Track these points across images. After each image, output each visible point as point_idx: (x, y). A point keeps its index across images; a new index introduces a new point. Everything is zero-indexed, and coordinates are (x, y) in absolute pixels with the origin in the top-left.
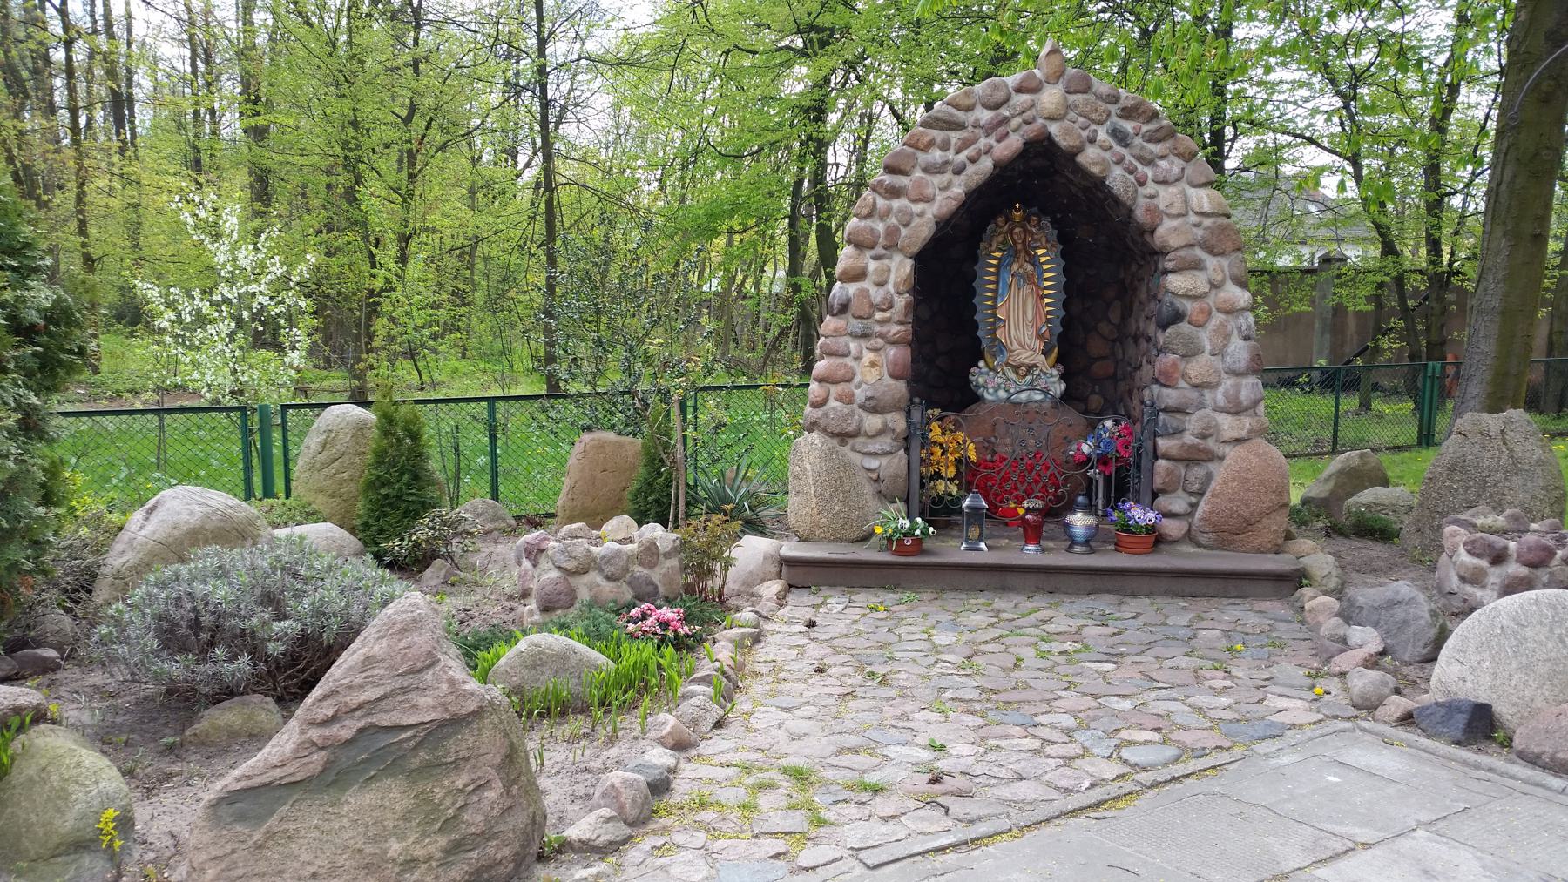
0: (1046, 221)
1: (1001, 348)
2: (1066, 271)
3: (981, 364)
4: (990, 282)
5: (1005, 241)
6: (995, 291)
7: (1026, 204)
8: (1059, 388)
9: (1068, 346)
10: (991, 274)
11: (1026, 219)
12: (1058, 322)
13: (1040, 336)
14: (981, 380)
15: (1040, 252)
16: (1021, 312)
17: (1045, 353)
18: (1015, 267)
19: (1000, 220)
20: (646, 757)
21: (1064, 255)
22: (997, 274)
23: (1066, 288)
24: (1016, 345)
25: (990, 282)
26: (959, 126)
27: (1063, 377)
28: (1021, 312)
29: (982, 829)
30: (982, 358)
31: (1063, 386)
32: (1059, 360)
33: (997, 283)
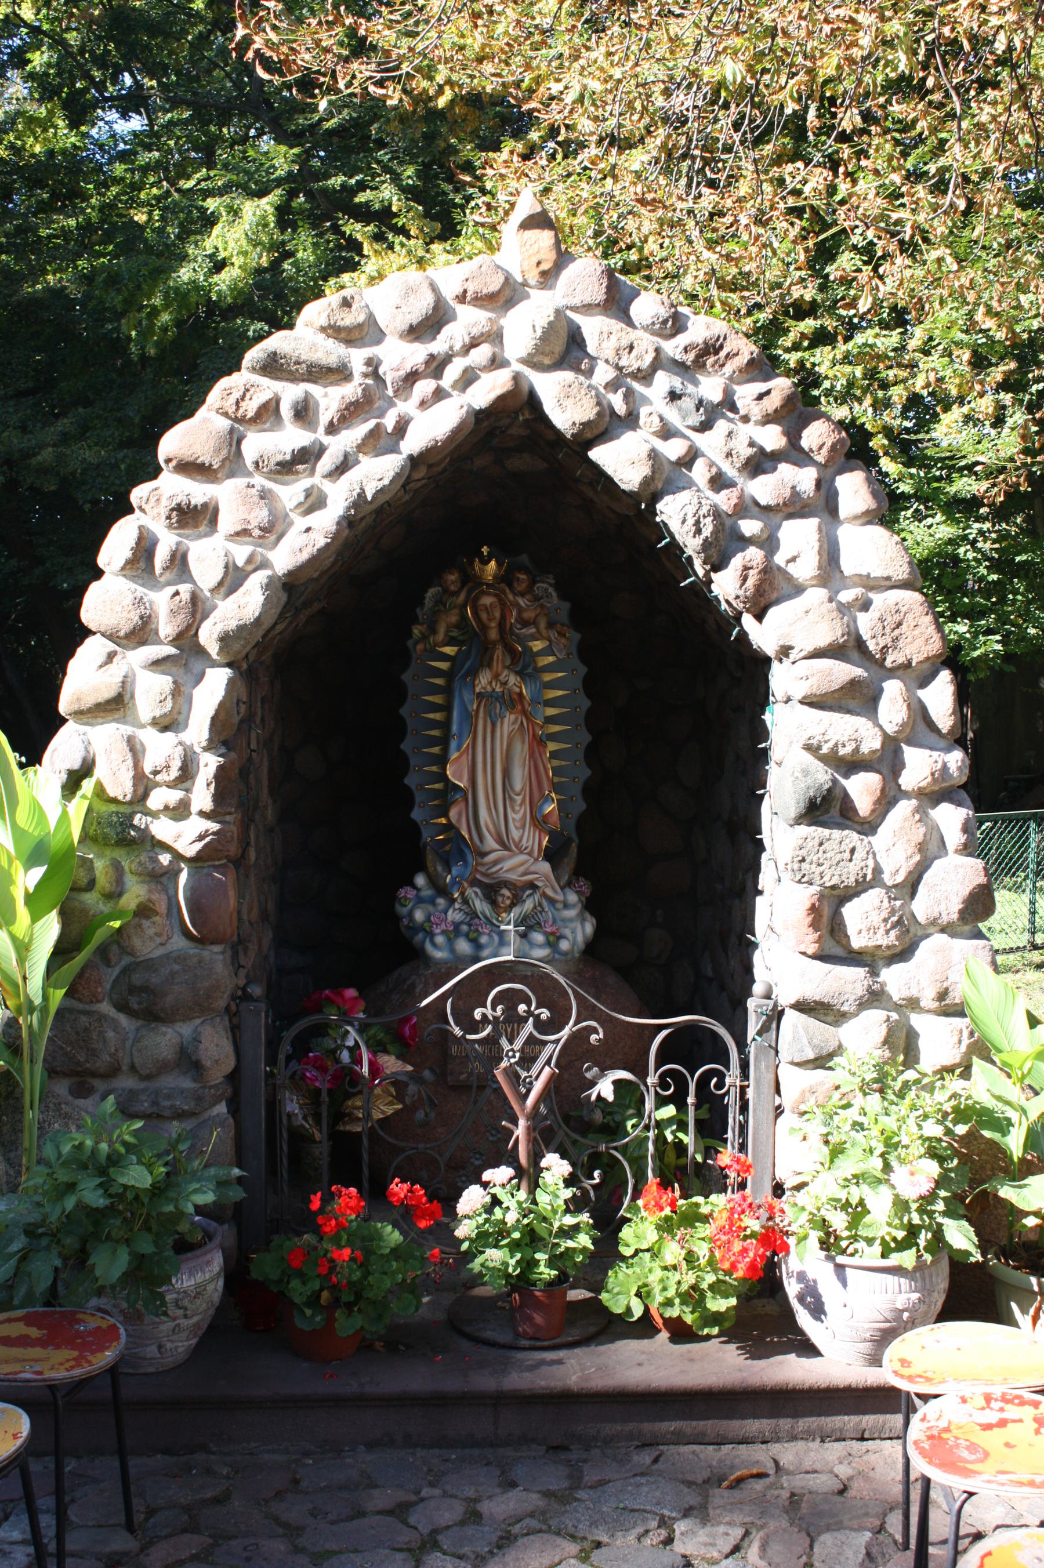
0: (545, 586)
1: (457, 848)
2: (590, 686)
3: (420, 880)
4: (435, 708)
5: (463, 623)
6: (445, 725)
7: (503, 550)
8: (579, 931)
9: (594, 850)
10: (436, 690)
11: (505, 578)
12: (577, 790)
13: (539, 822)
14: (419, 916)
15: (537, 645)
16: (503, 783)
17: (551, 855)
18: (483, 680)
19: (452, 578)
20: (579, 1547)
21: (584, 652)
22: (448, 691)
23: (591, 720)
24: (491, 843)
25: (435, 708)
26: (340, 373)
27: (590, 906)
28: (503, 783)
29: (539, 1344)
30: (422, 868)
31: (589, 928)
32: (578, 872)
33: (447, 708)
